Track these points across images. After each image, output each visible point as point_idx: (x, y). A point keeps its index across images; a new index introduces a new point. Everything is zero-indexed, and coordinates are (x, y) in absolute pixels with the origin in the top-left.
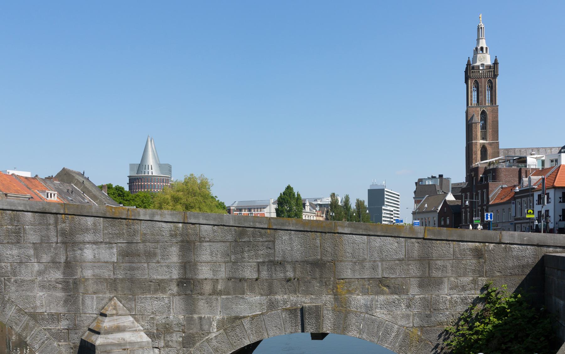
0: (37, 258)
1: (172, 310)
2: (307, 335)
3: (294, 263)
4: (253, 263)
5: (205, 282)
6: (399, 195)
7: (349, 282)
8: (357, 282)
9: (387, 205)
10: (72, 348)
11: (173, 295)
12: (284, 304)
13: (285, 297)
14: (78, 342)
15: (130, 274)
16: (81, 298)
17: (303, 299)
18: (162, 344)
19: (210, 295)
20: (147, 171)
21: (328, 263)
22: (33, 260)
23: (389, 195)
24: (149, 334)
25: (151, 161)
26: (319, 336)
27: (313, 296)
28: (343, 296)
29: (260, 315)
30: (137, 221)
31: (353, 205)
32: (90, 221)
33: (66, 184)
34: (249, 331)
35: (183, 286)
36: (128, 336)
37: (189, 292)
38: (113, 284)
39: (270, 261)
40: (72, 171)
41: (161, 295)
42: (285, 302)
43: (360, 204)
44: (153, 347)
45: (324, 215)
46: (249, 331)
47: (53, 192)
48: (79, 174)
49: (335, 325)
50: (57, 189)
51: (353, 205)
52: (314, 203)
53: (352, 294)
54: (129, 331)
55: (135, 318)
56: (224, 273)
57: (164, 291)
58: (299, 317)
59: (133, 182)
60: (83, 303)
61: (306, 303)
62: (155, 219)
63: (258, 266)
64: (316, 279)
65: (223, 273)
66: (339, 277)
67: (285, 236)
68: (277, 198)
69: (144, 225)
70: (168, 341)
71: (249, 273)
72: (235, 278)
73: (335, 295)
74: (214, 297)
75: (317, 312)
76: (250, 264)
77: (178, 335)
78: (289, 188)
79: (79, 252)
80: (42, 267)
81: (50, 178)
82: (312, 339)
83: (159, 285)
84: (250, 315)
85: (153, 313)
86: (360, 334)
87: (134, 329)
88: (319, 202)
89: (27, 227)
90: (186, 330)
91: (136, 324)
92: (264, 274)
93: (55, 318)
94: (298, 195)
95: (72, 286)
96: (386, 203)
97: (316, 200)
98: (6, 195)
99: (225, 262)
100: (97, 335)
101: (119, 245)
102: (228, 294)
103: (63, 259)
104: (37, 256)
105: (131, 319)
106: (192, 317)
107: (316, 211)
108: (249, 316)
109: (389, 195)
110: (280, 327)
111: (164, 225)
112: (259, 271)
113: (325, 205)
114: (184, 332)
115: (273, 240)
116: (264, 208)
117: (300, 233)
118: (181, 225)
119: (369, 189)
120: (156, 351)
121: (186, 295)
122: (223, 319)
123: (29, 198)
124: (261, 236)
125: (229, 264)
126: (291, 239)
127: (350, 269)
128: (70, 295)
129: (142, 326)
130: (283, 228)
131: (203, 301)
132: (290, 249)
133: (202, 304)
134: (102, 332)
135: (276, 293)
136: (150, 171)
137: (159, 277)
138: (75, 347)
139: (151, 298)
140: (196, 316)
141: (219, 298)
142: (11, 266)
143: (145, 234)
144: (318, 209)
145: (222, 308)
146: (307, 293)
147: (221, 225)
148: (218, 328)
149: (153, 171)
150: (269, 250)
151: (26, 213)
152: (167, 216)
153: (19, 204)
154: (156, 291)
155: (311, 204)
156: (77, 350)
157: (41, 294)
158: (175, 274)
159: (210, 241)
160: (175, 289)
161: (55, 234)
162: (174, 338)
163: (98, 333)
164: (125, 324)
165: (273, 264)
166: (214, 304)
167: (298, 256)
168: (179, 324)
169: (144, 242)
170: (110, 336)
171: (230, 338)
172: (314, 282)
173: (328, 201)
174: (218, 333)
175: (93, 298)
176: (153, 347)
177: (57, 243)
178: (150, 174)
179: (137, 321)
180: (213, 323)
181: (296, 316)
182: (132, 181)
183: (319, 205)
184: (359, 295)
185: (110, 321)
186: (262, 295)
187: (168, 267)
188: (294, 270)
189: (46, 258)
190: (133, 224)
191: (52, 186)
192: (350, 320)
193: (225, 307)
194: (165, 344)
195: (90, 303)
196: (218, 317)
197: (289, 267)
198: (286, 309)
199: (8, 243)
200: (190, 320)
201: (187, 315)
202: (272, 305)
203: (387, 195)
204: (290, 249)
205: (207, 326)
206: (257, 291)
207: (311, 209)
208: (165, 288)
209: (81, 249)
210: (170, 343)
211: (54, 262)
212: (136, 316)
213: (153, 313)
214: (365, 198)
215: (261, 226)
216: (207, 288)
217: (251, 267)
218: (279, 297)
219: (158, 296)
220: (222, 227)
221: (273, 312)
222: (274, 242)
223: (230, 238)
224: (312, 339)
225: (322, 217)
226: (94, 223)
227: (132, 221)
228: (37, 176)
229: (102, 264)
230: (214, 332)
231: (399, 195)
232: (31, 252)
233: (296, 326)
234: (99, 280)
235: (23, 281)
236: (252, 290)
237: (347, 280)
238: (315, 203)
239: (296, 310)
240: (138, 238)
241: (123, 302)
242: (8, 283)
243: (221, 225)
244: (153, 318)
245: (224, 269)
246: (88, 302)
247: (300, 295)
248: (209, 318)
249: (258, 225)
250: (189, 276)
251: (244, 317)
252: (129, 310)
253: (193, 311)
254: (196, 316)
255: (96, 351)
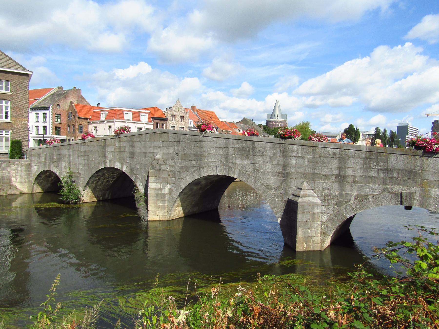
0: (271, 162)
1: (332, 189)
2: (403, 207)
3: (398, 171)
4: (375, 169)
5: (349, 177)
6: (417, 129)
7: (430, 182)
8: (435, 182)
9: (409, 135)
10: (284, 202)
11: (333, 182)
12: (391, 190)
13: (392, 187)
14: (287, 200)
15: (313, 171)
16: (289, 180)
17: (402, 189)
18: (326, 204)
19: (352, 183)
20: (275, 117)
21: (418, 172)
22: (269, 163)
23: (411, 129)
24: (321, 200)
25: (277, 113)
26: (408, 208)
27: (408, 187)
28: (426, 189)
29: (378, 194)
30: (317, 147)
31: (388, 134)
32: (295, 147)
33: (245, 125)
34: (371, 202)
35: (338, 178)
36: (312, 199)
37: (341, 181)
38: (305, 175)
39: (385, 169)
40: (247, 119)
41: (327, 182)
42: (392, 189)
43: (392, 134)
44: (322, 205)
45: (370, 141)
46: (371, 202)
47: (240, 129)
48: (250, 120)
49: (421, 203)
50: (242, 128)
51: (388, 134)
52: (364, 134)
53: (432, 188)
54: (311, 197)
55: (314, 191)
56: (359, 173)
57: (329, 179)
58: (400, 198)
59: (268, 123)
60: (290, 183)
61: (404, 191)
62: (326, 147)
63: (378, 171)
64: (410, 179)
65: (359, 173)
66: (424, 179)
67: (393, 157)
68: (295, 125)
69: (321, 149)
70: (330, 203)
71: (373, 174)
72: (365, 176)
73: (422, 188)
74: (354, 184)
75: (411, 196)
76: (374, 169)
77: (335, 201)
78: (351, 126)
79: (290, 160)
80: (273, 166)
81: (238, 123)
82: (405, 209)
83: (326, 177)
84: (372, 194)
85: (322, 189)
86: (436, 209)
87: (314, 196)
88: (367, 133)
89: (267, 149)
90: (339, 199)
91: (314, 193)
92: (381, 175)
93: (277, 188)
94: (357, 129)
95: (286, 175)
96: (408, 134)
97: (366, 132)
98: (222, 130)
99: (360, 168)
100: (298, 198)
101: (308, 158)
102: (361, 183)
103: (282, 163)
104: (271, 161)
105: (312, 191)
106: (342, 193)
107: (366, 138)
108: (372, 195)
109: (411, 129)
110: (389, 202)
111: (330, 149)
112: (378, 173)
113: (371, 135)
114: (338, 200)
115: (387, 158)
116: (337, 136)
117: (403, 155)
118: (339, 150)
119: (398, 125)
120: (323, 207)
121: (339, 182)
122: (358, 195)
123: (231, 132)
124: (381, 156)
125: (362, 169)
126: (397, 158)
127: (432, 175)
128: (284, 179)
129: (317, 195)
130: (393, 153)
131: (348, 186)
132: (396, 163)
133: (347, 187)
134: (301, 196)
135: (387, 185)
136: (277, 117)
137: (327, 173)
138: (285, 202)
139: (322, 183)
140: (344, 193)
141: (356, 185)
142: (259, 165)
143: (321, 153)
144: (367, 137)
145: (357, 189)
146: (404, 186)
147: (359, 150)
148: (355, 199)
149: (278, 117)
150: (385, 163)
151: (267, 143)
152: (332, 146)
153: (264, 139)
154: (324, 180)
155: (363, 135)
156: (286, 203)
157: (272, 178)
158: (335, 172)
159: (353, 158)
160: (334, 179)
161: (279, 152)
162: (333, 202)
163: (299, 197)
164: (310, 194)
165: (387, 170)
166: (354, 187)
167: (400, 167)
168: (335, 196)
169: (320, 157)
170: (304, 199)
171: (361, 204)
172: (409, 180)
173: (373, 132)
174: (355, 201)
175: (295, 181)
176: (322, 205)
177: (280, 156)
178: (277, 119)
179: (315, 193)
180: (353, 196)
181: (398, 197)
182: (268, 122)
183: (367, 135)
184: (436, 189)
185: (303, 192)
186: (379, 185)
187: (331, 169)
188: (398, 174)
189: (275, 162)
190: (315, 149)
191: (240, 126)
192: (430, 201)
193: (359, 190)
194: (328, 204)
195: (293, 183)
196: (355, 194)
197: (395, 172)
198: (392, 193)
199: (259, 155)
200: (341, 194)
201: (339, 192)
202: (384, 191)
203: (410, 129)
204: (396, 163)
205: (349, 198)
206: (377, 183)
207: (363, 137)
208: (329, 179)
209: (290, 159)
210: (330, 204)
211: (278, 164)
212: (315, 190)
213: (322, 189)
214: (395, 130)
215: (381, 152)
216: (351, 180)
217: (374, 171)
218: (389, 187)
219: (326, 182)
220: (359, 151)
221: (385, 194)
222: (387, 159)
223: (363, 156)
224: (405, 209)
225: (369, 141)
226: (297, 148)
227: (315, 147)
228: (233, 122)
229: (299, 166)
230: (353, 201)
231: (417, 129)
232: (269, 159)
233: (397, 202)
234: (297, 173)
235: (264, 172)
236: (374, 183)
237: (429, 181)
238: (365, 134)
239: (398, 193)
240: (317, 155)
241: (309, 183)
242: (258, 173)
243: (359, 150)
244: (322, 192)
245: (359, 171)
246: (293, 183)
247: (401, 186)
248: (350, 194)
249: (379, 151)
250: (342, 173)
251: (369, 195)
252: (311, 187)
253: (343, 190)
254: (344, 193)
255: (298, 204)
